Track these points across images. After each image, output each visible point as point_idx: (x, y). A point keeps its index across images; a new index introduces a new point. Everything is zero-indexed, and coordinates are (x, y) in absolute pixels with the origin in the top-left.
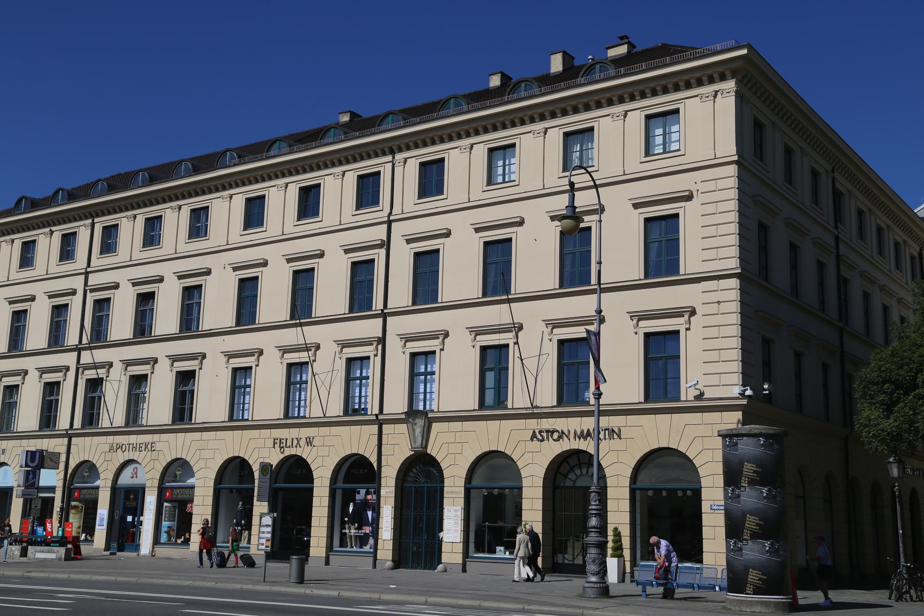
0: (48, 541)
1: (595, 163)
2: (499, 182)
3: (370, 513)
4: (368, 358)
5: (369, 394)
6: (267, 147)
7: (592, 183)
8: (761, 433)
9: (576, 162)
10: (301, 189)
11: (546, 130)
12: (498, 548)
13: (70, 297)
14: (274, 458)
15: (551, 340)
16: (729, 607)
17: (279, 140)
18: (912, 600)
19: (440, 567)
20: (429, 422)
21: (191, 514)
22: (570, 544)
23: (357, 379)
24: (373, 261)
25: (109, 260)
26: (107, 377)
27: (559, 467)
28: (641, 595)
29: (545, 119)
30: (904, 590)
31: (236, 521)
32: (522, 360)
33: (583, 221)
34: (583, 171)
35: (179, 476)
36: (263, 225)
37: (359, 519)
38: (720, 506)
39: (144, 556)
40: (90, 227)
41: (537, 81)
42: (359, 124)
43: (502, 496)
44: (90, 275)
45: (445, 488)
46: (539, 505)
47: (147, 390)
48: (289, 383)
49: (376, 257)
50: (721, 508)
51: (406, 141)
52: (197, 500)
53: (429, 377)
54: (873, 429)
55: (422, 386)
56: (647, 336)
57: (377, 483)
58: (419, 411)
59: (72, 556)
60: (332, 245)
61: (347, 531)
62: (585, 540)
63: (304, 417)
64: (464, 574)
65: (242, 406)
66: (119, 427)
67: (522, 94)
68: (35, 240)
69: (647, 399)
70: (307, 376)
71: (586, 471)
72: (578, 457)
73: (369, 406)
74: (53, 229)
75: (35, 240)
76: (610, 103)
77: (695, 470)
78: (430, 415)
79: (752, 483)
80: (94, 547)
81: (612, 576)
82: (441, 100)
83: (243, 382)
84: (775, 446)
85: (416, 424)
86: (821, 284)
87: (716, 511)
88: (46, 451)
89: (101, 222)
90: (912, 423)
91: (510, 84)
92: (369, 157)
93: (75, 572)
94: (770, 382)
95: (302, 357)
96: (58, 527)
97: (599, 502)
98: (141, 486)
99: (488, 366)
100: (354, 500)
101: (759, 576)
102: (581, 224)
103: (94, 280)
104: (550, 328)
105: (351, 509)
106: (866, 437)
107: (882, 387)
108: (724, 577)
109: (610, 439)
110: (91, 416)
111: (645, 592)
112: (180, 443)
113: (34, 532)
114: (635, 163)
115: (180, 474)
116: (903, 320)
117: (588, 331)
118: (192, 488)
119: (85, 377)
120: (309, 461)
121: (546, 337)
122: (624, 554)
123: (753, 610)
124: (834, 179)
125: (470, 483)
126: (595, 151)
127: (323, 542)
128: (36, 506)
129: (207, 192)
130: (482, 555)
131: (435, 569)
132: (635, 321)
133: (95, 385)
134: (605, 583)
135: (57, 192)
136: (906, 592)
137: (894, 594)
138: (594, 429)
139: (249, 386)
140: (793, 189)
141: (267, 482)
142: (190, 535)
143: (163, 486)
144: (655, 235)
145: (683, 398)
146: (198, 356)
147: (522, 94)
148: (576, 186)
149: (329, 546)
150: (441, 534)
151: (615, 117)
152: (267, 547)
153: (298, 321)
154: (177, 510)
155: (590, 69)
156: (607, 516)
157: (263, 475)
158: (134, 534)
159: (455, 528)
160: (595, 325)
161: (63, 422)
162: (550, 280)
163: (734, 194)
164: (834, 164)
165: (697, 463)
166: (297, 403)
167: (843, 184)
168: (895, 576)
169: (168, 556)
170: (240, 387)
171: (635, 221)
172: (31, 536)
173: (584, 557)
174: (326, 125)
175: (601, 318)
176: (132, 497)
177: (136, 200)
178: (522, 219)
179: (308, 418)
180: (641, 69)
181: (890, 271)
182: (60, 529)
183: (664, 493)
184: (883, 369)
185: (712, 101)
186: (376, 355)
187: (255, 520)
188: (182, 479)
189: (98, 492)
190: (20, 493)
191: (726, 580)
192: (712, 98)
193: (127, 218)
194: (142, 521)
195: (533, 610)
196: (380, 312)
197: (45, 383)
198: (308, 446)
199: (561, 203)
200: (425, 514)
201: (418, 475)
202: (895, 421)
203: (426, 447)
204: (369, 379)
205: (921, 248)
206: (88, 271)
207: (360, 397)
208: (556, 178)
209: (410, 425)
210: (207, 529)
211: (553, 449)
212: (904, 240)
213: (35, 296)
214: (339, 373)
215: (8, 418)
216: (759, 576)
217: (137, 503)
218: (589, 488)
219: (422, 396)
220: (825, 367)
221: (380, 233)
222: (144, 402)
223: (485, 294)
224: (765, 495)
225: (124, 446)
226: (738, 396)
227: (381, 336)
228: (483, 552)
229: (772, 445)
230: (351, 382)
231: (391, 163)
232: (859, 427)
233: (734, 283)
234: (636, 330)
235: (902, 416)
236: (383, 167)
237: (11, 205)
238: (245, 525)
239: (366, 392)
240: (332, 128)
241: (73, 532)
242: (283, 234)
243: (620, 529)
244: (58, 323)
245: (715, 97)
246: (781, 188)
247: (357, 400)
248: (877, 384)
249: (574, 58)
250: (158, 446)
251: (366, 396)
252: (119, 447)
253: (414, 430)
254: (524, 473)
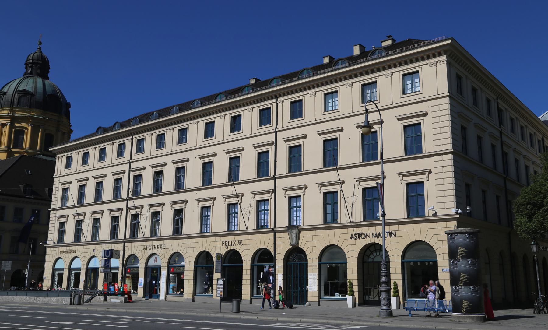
0: (116, 293)
1: (378, 99)
2: (330, 110)
3: (271, 278)
4: (268, 200)
5: (269, 218)
6: (215, 97)
7: (377, 109)
8: (467, 232)
9: (368, 99)
10: (232, 117)
11: (353, 83)
12: (336, 294)
13: (104, 178)
14: (223, 251)
15: (359, 188)
16: (454, 320)
17: (276, 78)
18: (545, 313)
19: (307, 304)
20: (299, 231)
21: (183, 280)
22: (372, 290)
23: (262, 210)
24: (268, 151)
25: (140, 156)
26: (141, 213)
27: (365, 251)
28: (408, 315)
29: (413, 63)
30: (541, 308)
31: (205, 283)
32: (345, 199)
33: (373, 128)
34: (372, 103)
35: (177, 261)
36: (214, 136)
37: (265, 280)
38: (447, 269)
39: (162, 300)
40: (131, 140)
41: (347, 60)
42: (260, 84)
43: (337, 268)
44: (131, 163)
45: (308, 264)
46: (356, 271)
47: (160, 219)
48: (229, 214)
49: (270, 150)
50: (448, 270)
51: (295, 88)
52: (186, 273)
53: (298, 208)
54: (523, 227)
55: (295, 213)
56: (407, 184)
57: (274, 262)
58: (294, 226)
59: (128, 300)
60: (248, 144)
61: (260, 287)
62: (379, 288)
63: (237, 230)
65: (206, 225)
66: (147, 237)
67: (340, 66)
68: (88, 152)
69: (409, 216)
70: (238, 210)
71: (379, 253)
72: (375, 246)
73: (269, 224)
74: (114, 142)
75: (88, 152)
76: (384, 69)
77: (434, 251)
78: (300, 228)
79: (463, 257)
80: (138, 296)
81: (394, 306)
82: (300, 71)
83: (206, 214)
84: (474, 238)
85: (292, 232)
86: (494, 156)
87: (445, 272)
88: (114, 250)
89: (136, 138)
90: (542, 224)
91: (334, 62)
92: (265, 100)
93: (129, 308)
94: (470, 206)
95: (235, 200)
96: (121, 287)
97: (386, 269)
98: (159, 266)
99: (328, 202)
100: (263, 271)
101: (468, 304)
102: (372, 130)
103: (134, 166)
104: (358, 182)
105: (262, 275)
106: (519, 232)
107: (526, 206)
108: (450, 305)
109: (391, 237)
110: (134, 233)
111: (411, 313)
112: (177, 245)
113: (109, 289)
114: (398, 98)
115: (177, 260)
116: (535, 172)
117: (377, 183)
118: (184, 266)
119: (131, 214)
120: (240, 252)
121: (356, 187)
122: (399, 295)
123: (465, 321)
124: (498, 103)
125: (320, 261)
126: (378, 93)
127: (248, 292)
128: (110, 277)
129: (180, 122)
130: (328, 297)
131: (305, 304)
132: (401, 177)
133: (135, 217)
134: (390, 309)
135: (115, 124)
136: (542, 309)
137: (536, 311)
138: (382, 232)
139: (210, 216)
140: (478, 109)
141: (220, 263)
142: (183, 290)
143: (169, 266)
144: (409, 134)
145: (427, 215)
147: (340, 66)
148: (369, 111)
149: (251, 294)
150: (307, 287)
151: (387, 76)
152: (221, 295)
153: (232, 183)
154: (177, 278)
155: (373, 52)
156: (390, 276)
157: (218, 260)
158: (156, 290)
159: (314, 284)
160: (381, 180)
161: (121, 236)
162: (357, 158)
163: (448, 112)
164: (497, 96)
165: (435, 248)
166: (233, 223)
167: (503, 106)
168: (536, 301)
169: (173, 300)
170: (205, 216)
171: (399, 127)
172: (108, 291)
173: (379, 297)
174: (243, 85)
175: (384, 176)
176: (155, 271)
177: (152, 126)
178: (342, 128)
179: (340, 223)
180: (399, 52)
181: (528, 148)
182: (121, 287)
183: (419, 264)
184: (527, 197)
185: (435, 66)
186: (271, 199)
187: (215, 282)
188: (178, 262)
189: (139, 269)
190: (102, 270)
191: (451, 306)
192: (435, 65)
193: (149, 135)
194: (160, 283)
195: (354, 324)
196: (273, 177)
197: (60, 223)
198: (239, 244)
199: (361, 119)
200: (298, 277)
201: (294, 258)
202: (534, 223)
203: (298, 244)
204: (301, 207)
205: (543, 136)
206: (277, 130)
207: (264, 219)
208: (358, 107)
209: (289, 233)
210: (267, 288)
211: (362, 243)
212: (534, 132)
213: (106, 175)
214: (254, 208)
215: (96, 234)
216: (468, 304)
217: (157, 275)
218: (381, 262)
219: (295, 218)
220: (498, 197)
221: (272, 137)
222: (159, 225)
223: (325, 167)
224: (470, 263)
225: (150, 247)
226: (454, 213)
227: (274, 189)
228: (328, 295)
229: (472, 237)
230: (260, 212)
231: (276, 103)
232: (516, 227)
233: (450, 156)
234: (401, 182)
235: (537, 221)
236: (421, 68)
237: (94, 131)
238: (209, 285)
239: (267, 217)
240: (246, 86)
241: (128, 289)
242: (224, 140)
243: (397, 282)
244: (117, 187)
245: (437, 64)
246: (472, 108)
247: (263, 221)
248: (524, 205)
249: (365, 48)
250: (166, 247)
251: (267, 219)
252: (148, 247)
253: (292, 235)
254: (347, 255)
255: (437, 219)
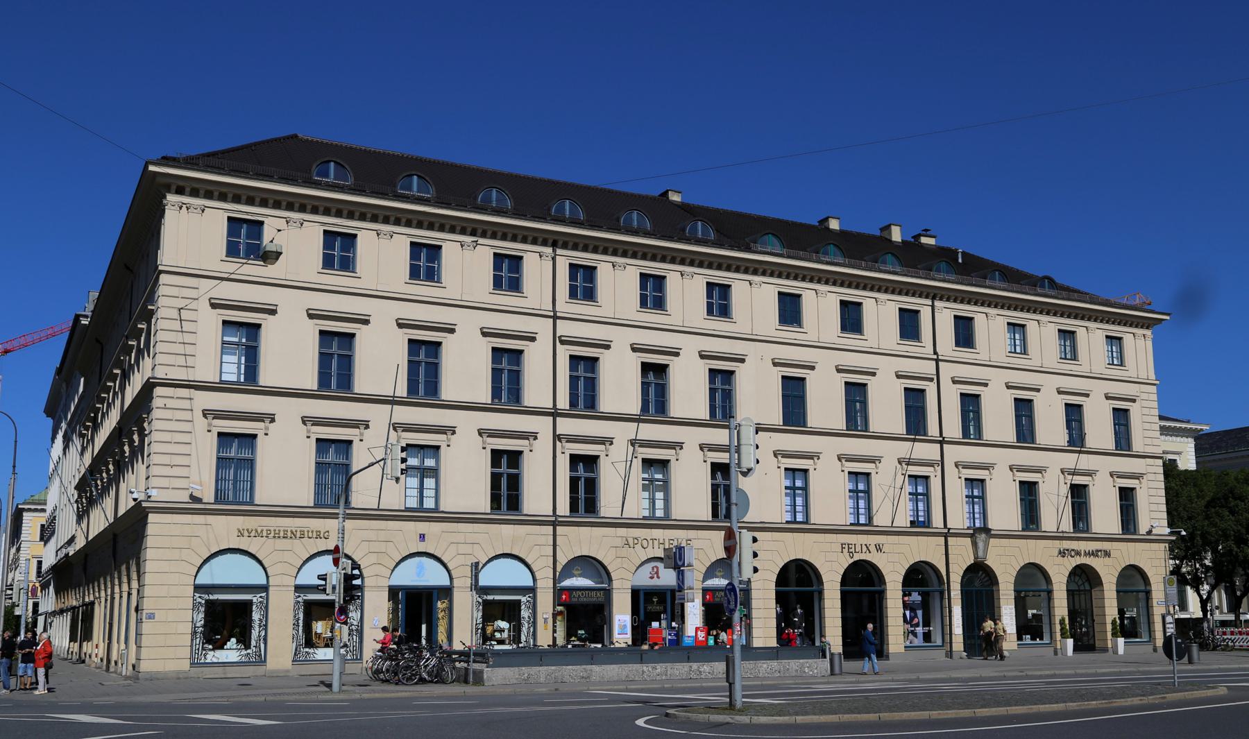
29: (399, 225)
60: (826, 362)
64: (1155, 653)
146: (265, 418)
176: (655, 600)
255: (1150, 538)
